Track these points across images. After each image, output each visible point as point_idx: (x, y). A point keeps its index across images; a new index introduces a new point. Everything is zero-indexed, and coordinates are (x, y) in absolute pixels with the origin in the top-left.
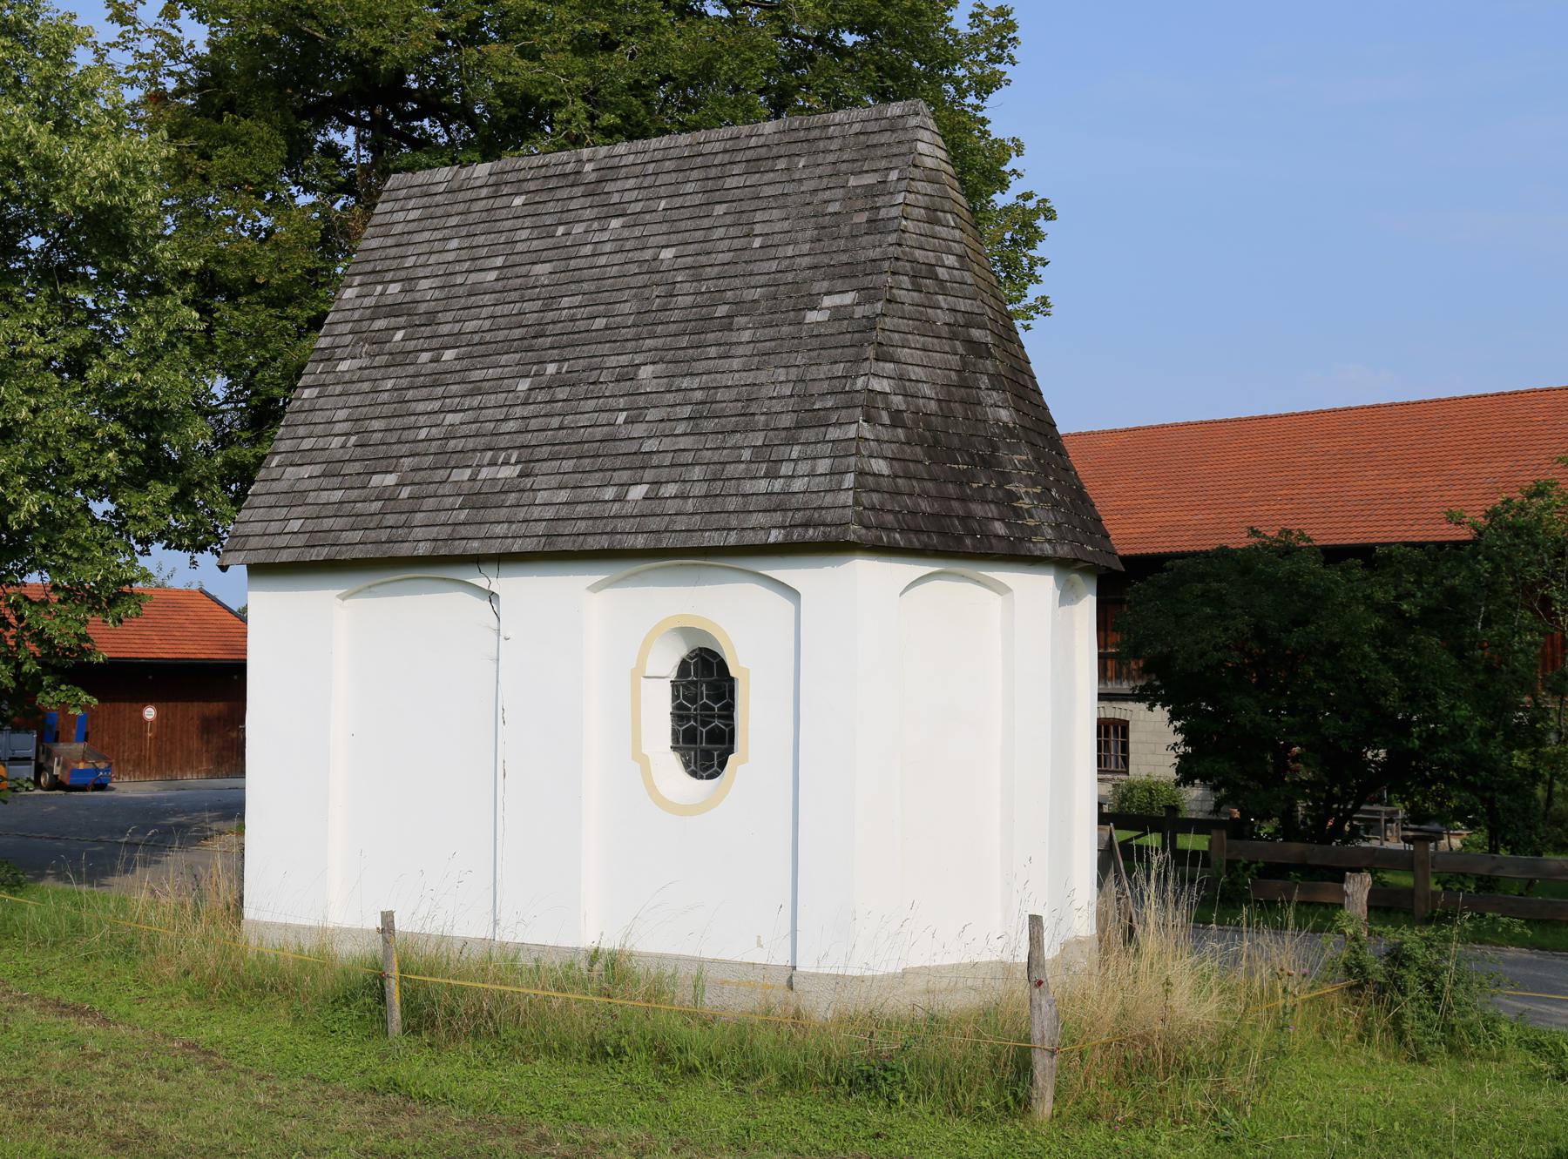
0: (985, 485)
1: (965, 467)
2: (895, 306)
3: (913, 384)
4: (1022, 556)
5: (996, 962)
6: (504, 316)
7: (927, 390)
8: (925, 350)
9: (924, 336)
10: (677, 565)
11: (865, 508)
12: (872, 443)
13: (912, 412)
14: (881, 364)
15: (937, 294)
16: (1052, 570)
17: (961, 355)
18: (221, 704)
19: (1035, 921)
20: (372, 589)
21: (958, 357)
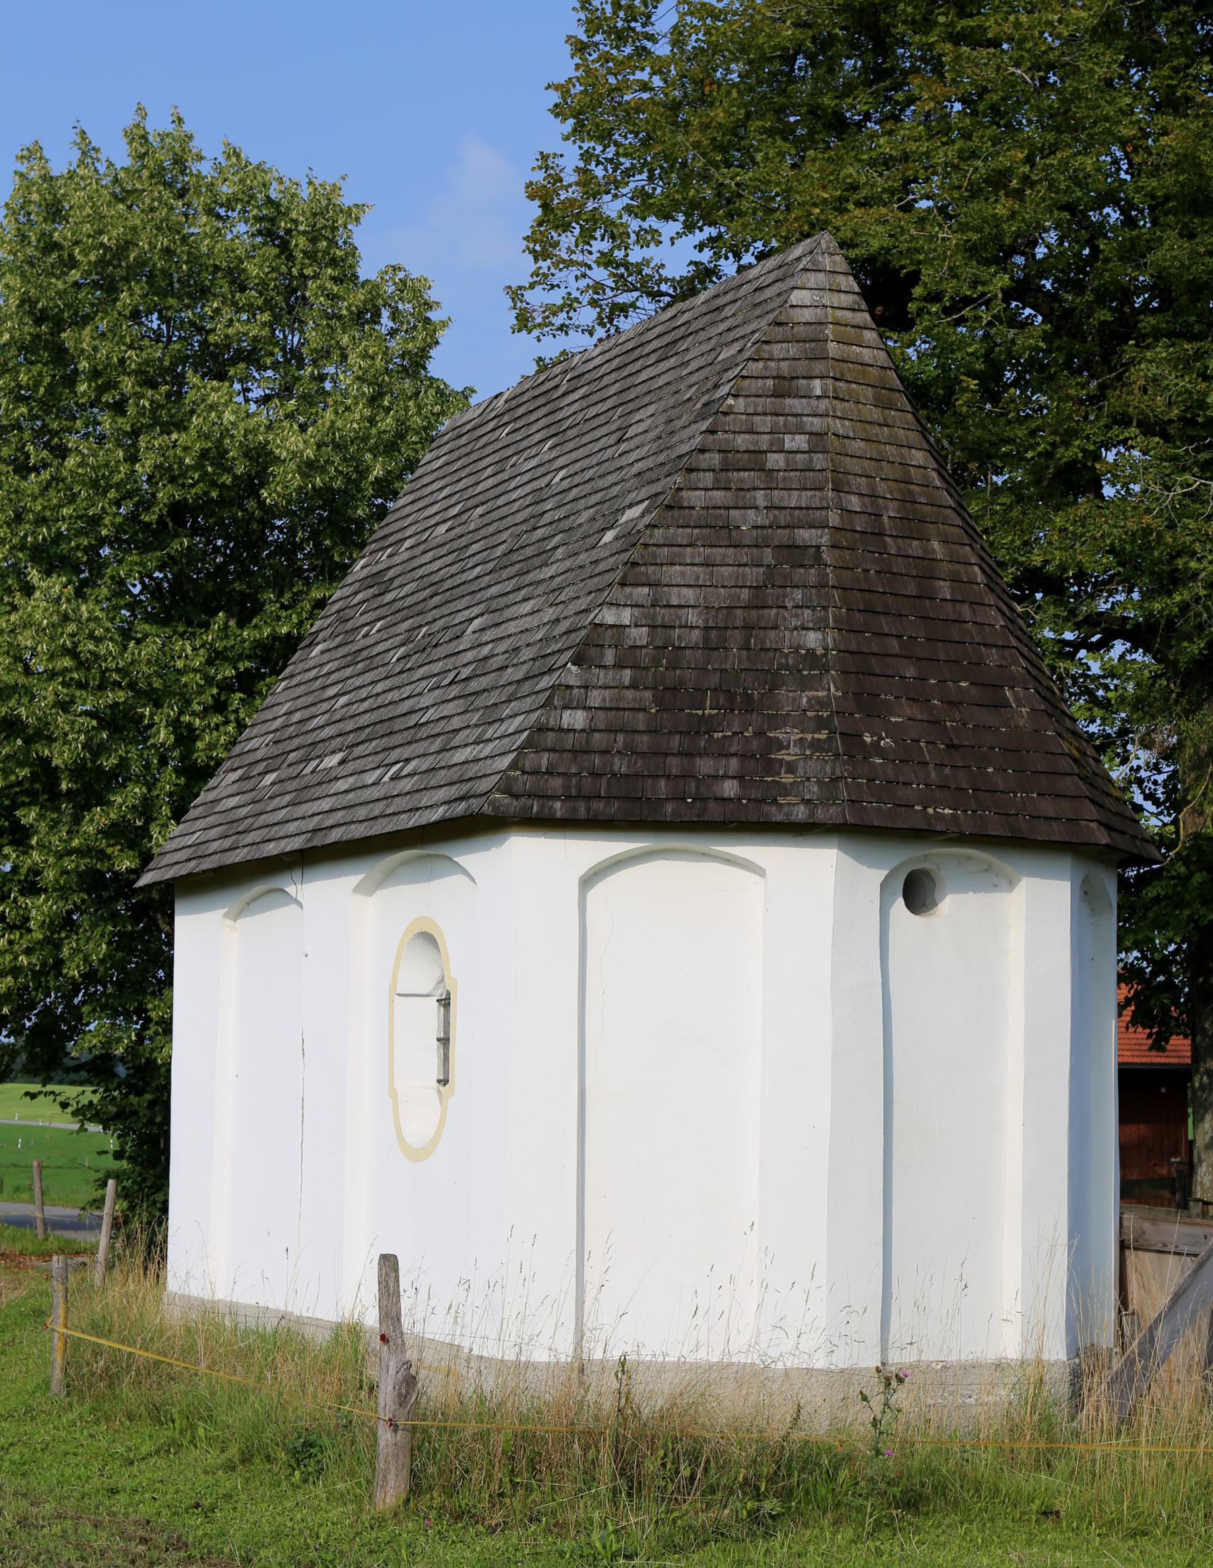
0: (735, 733)
1: (716, 711)
2: (676, 513)
3: (672, 610)
4: (776, 823)
5: (828, 1372)
6: (800, 508)
7: (692, 617)
8: (708, 565)
9: (711, 546)
10: (421, 857)
11: (524, 772)
12: (576, 691)
13: (656, 648)
14: (628, 590)
15: (755, 489)
16: (835, 840)
17: (768, 566)
18: (1142, 1127)
19: (389, 1264)
20: (251, 906)
21: (762, 570)
